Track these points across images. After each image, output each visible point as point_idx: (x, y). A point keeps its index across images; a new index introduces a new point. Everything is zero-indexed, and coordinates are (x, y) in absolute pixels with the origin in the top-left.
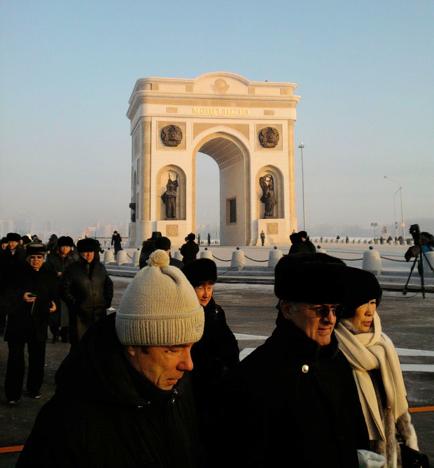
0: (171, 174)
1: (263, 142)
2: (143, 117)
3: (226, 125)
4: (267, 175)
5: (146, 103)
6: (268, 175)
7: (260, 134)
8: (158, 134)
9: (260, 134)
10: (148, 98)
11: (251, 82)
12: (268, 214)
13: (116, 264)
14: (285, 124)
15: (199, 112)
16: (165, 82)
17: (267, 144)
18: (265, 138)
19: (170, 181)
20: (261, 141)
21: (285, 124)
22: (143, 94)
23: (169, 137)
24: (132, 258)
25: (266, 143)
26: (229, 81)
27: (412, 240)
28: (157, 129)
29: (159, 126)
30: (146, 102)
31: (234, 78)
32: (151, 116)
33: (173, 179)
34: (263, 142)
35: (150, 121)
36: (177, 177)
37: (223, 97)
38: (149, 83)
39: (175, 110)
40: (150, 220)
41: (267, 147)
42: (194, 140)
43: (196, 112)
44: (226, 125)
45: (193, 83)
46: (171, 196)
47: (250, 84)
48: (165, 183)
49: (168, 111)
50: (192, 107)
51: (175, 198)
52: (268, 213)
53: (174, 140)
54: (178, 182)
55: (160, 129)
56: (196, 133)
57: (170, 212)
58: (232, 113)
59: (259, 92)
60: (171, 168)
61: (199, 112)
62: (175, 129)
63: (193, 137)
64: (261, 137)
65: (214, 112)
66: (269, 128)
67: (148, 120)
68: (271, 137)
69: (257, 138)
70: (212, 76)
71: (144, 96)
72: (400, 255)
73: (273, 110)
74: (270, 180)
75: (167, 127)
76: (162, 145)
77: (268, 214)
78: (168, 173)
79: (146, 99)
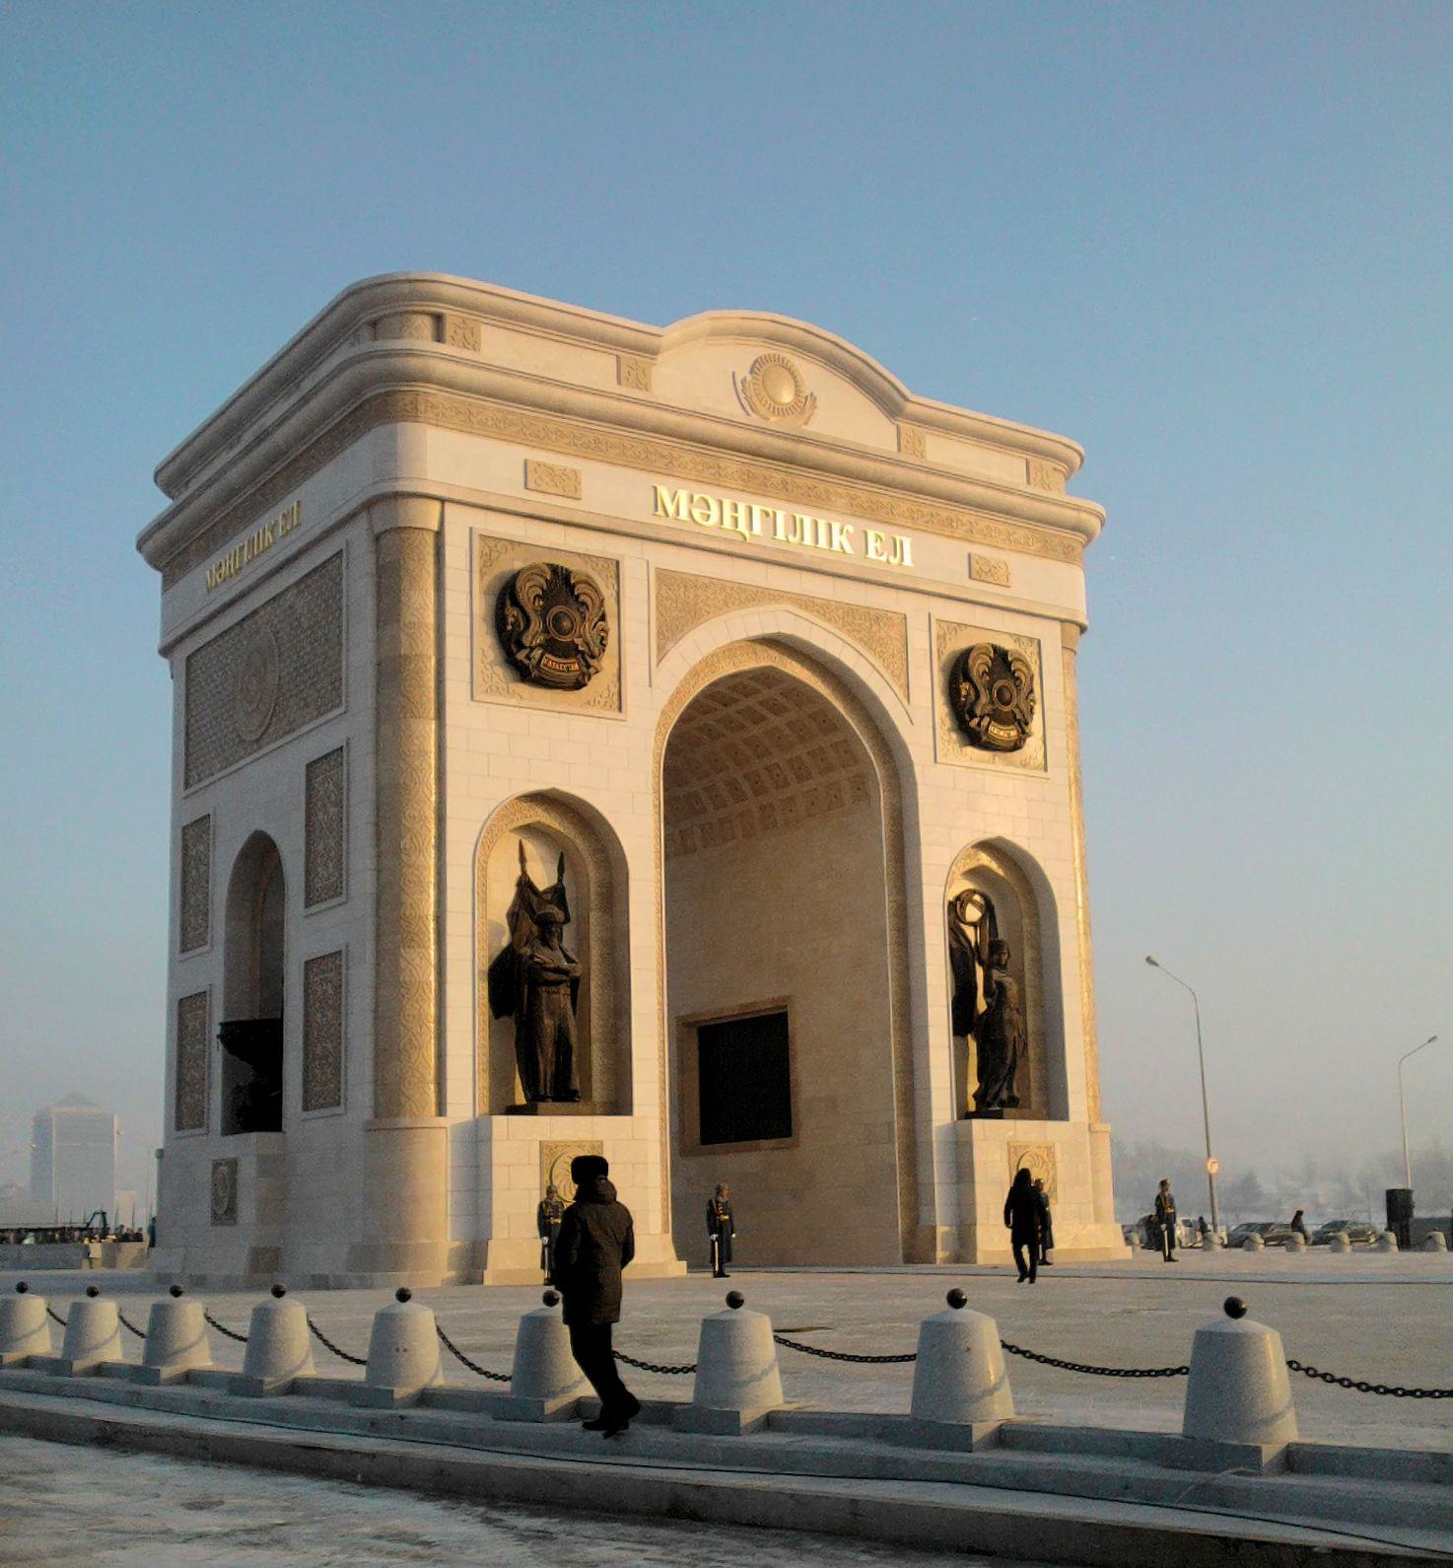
0: (531, 848)
1: (521, 646)
2: (398, 495)
3: (805, 602)
4: (968, 890)
5: (415, 419)
6: (974, 892)
7: (506, 594)
8: (482, 606)
9: (504, 588)
10: (431, 389)
11: (920, 402)
12: (1004, 1095)
13: (243, 1386)
14: (639, 566)
15: (684, 515)
16: (513, 320)
17: (991, 728)
18: (536, 625)
19: (525, 885)
20: (508, 641)
21: (1051, 636)
22: (405, 359)
23: (992, 702)
24: (142, 1335)
25: (537, 653)
26: (812, 374)
27: (536, 1189)
28: (476, 576)
29: (488, 561)
30: (412, 415)
31: (834, 363)
32: (443, 501)
33: (543, 877)
34: (521, 646)
35: (435, 527)
36: (561, 870)
37: (803, 450)
38: (426, 309)
39: (568, 484)
40: (441, 1110)
41: (989, 746)
42: (658, 664)
43: (671, 509)
44: (805, 602)
45: (653, 352)
46: (558, 970)
47: (909, 408)
48: (504, 896)
49: (531, 485)
50: (654, 479)
51: (576, 985)
52: (1000, 1090)
53: (569, 651)
54: (569, 895)
55: (488, 579)
56: (669, 630)
57: (546, 1067)
58: (836, 547)
59: (940, 451)
60: (539, 811)
61: (684, 515)
62: (572, 588)
63: (658, 646)
64: (512, 613)
65: (757, 529)
66: (554, 569)
67: (427, 516)
68: (566, 624)
69: (485, 620)
70: (745, 334)
71: (410, 378)
72: (823, 1280)
73: (575, 467)
74: (982, 919)
75: (533, 570)
76: (500, 674)
77: (1004, 1095)
78: (515, 839)
79: (417, 393)
